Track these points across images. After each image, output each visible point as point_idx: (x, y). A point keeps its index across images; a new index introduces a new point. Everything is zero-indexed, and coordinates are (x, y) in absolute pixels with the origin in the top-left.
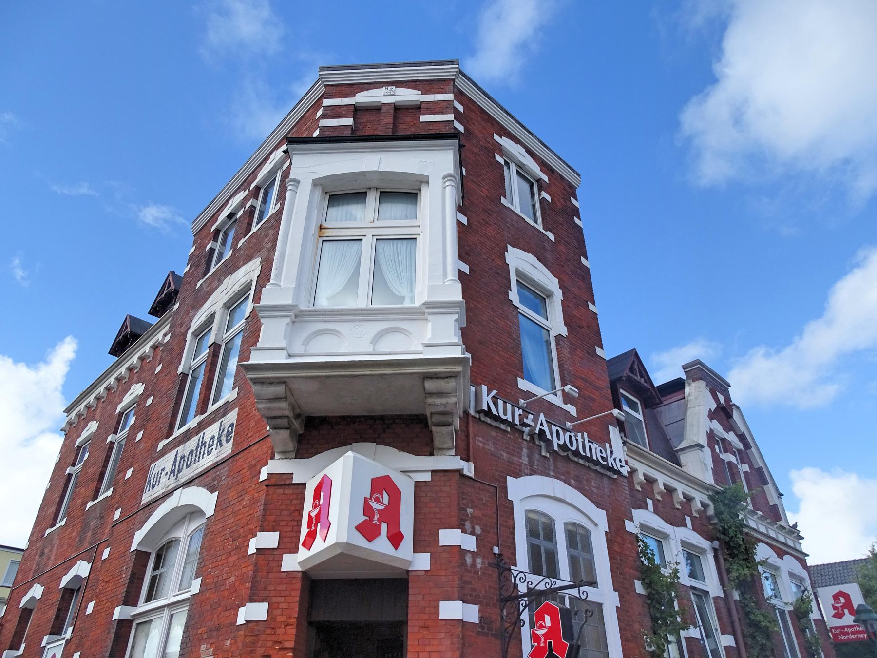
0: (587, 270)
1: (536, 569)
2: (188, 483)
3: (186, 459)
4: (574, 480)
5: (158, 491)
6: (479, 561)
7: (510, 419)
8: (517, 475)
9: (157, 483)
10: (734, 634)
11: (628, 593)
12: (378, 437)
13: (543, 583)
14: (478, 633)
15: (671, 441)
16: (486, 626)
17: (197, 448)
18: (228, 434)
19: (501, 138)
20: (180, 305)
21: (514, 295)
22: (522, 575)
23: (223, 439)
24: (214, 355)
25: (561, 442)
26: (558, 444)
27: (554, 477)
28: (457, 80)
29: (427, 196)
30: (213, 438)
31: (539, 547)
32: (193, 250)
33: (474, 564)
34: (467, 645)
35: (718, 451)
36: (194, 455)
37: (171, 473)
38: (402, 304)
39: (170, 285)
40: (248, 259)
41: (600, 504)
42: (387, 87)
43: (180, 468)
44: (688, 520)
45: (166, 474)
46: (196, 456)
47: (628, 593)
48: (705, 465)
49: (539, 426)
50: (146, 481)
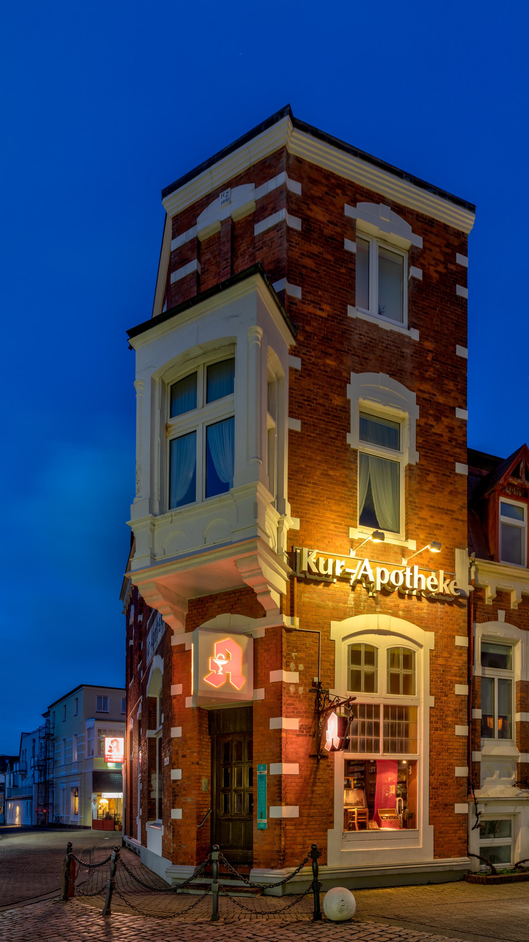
12: (232, 608)
14: (298, 735)
16: (305, 731)
25: (384, 582)
27: (380, 612)
28: (291, 145)
29: (401, 323)
31: (359, 672)
33: (296, 692)
34: (289, 743)
38: (501, 514)
41: (429, 627)
42: (223, 193)
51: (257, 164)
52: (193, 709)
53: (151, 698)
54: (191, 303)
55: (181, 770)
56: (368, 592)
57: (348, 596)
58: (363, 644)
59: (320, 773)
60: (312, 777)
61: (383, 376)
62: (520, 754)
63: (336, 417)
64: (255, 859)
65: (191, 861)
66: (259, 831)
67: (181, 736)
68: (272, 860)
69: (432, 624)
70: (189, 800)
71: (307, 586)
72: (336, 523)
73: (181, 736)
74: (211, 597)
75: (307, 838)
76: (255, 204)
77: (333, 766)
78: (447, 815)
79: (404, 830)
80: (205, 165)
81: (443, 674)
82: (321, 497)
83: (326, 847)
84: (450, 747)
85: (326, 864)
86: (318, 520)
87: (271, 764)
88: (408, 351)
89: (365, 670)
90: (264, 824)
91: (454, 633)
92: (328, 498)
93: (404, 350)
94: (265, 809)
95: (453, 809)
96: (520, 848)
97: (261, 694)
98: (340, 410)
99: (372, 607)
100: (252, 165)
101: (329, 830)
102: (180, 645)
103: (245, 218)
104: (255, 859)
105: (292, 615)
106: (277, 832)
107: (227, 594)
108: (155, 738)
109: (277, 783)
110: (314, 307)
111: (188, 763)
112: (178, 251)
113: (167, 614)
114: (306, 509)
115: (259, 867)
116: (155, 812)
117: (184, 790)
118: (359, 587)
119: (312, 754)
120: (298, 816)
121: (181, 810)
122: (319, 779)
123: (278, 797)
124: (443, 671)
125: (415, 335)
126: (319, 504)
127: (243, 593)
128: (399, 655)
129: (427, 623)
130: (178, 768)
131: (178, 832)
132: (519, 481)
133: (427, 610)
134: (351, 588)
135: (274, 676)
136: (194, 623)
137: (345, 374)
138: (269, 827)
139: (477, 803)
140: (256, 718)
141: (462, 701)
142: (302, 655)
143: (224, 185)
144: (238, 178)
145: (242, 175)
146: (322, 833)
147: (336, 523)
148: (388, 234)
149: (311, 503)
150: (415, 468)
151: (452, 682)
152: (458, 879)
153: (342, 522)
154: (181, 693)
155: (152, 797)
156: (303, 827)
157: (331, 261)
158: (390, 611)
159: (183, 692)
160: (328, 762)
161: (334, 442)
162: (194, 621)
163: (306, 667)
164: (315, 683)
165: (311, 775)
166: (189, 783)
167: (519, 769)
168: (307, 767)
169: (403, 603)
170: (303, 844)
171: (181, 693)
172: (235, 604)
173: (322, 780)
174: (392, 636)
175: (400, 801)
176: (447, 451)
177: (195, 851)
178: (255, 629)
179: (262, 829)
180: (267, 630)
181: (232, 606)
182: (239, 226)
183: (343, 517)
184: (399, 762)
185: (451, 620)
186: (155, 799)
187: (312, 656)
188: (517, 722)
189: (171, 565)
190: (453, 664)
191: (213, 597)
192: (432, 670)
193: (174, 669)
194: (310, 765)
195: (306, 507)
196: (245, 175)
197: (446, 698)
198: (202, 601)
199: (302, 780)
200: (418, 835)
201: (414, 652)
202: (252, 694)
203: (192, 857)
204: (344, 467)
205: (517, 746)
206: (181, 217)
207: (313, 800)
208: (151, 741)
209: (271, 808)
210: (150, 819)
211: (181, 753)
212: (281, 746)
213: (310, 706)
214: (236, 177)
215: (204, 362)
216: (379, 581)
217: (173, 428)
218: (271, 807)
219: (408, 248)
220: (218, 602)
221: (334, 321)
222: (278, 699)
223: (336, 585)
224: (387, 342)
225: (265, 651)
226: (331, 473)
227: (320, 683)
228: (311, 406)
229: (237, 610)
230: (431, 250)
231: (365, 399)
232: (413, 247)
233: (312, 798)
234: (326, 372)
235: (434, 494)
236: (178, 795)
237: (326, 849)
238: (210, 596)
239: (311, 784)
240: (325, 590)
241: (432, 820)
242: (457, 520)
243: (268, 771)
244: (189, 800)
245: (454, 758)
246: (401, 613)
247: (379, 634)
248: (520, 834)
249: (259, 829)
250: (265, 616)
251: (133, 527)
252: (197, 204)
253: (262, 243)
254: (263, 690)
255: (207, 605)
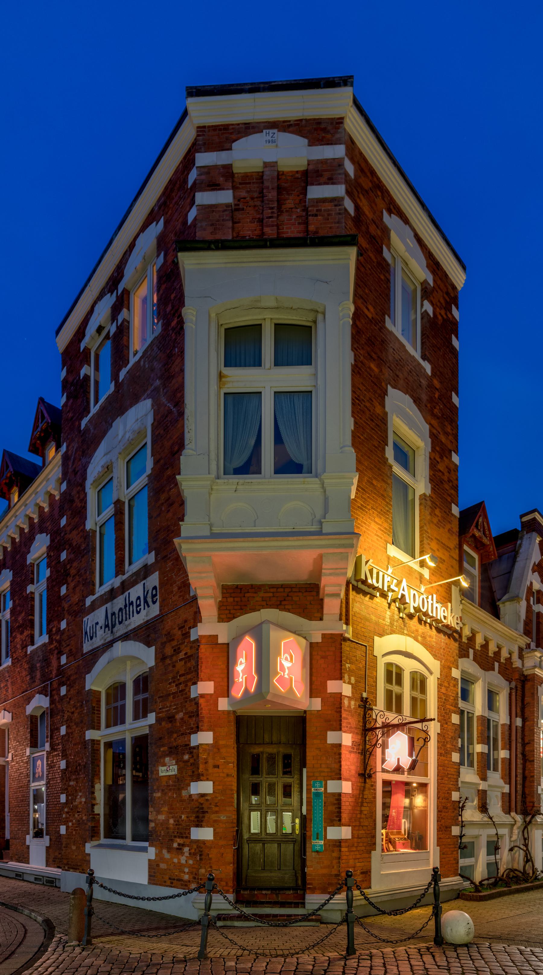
0: (454, 409)
1: (389, 708)
2: (125, 637)
3: (117, 616)
4: (421, 637)
5: (98, 642)
6: (353, 703)
7: (381, 587)
8: (381, 635)
9: (94, 635)
10: (510, 750)
11: (447, 723)
12: (280, 604)
13: (397, 719)
15: (495, 593)
17: (126, 606)
18: (154, 596)
19: (390, 216)
20: (67, 447)
21: (389, 453)
22: (382, 713)
23: (149, 600)
24: (119, 513)
25: (416, 605)
26: (414, 607)
30: (139, 598)
32: (64, 373)
35: (532, 603)
36: (124, 612)
37: (105, 628)
39: (43, 418)
40: (136, 399)
41: (436, 656)
42: (268, 131)
43: (114, 623)
44: (496, 665)
45: (101, 628)
46: (126, 614)
47: (447, 723)
48: (519, 616)
49: (401, 592)
50: (82, 633)
51: (310, 120)
52: (228, 712)
53: (95, 691)
54: (268, 243)
55: (211, 783)
56: (399, 612)
57: (386, 613)
58: (395, 664)
59: (366, 792)
60: (361, 796)
61: (408, 398)
62: (481, 782)
63: (378, 425)
64: (310, 884)
65: (226, 888)
66: (313, 854)
67: (212, 742)
68: (330, 884)
69: (438, 653)
70: (223, 818)
71: (358, 596)
72: (378, 536)
73: (212, 742)
74: (252, 586)
75: (357, 861)
76: (306, 163)
77: (375, 786)
78: (447, 837)
79: (417, 851)
80: (247, 87)
81: (444, 703)
82: (368, 505)
83: (371, 869)
84: (449, 772)
85: (370, 887)
86: (366, 528)
87: (328, 782)
88: (424, 382)
89: (396, 690)
90: (321, 845)
91: (451, 665)
92: (372, 508)
93: (421, 380)
94: (322, 830)
95: (451, 831)
96: (481, 866)
97: (317, 704)
98: (381, 420)
99: (402, 628)
100: (304, 118)
101: (372, 852)
102: (210, 636)
103: (292, 172)
104: (310, 884)
105: (347, 623)
106: (335, 854)
107: (272, 586)
108: (99, 741)
109: (336, 802)
110: (362, 303)
111: (221, 775)
112: (206, 170)
113: (205, 597)
114: (357, 514)
115: (314, 893)
116: (99, 830)
117: (216, 806)
118: (393, 606)
119: (361, 772)
120: (351, 838)
121: (211, 830)
122: (366, 799)
123: (337, 817)
124: (445, 699)
125: (428, 367)
126: (367, 512)
127: (294, 590)
128: (417, 679)
129: (435, 652)
130: (208, 780)
131: (208, 855)
132: (479, 533)
133: (436, 639)
134: (387, 605)
135: (332, 686)
136: (230, 613)
137: (383, 384)
138: (326, 850)
139: (464, 826)
140: (311, 729)
141: (456, 730)
142: (353, 667)
143: (269, 122)
144: (286, 124)
145: (292, 123)
146: (367, 855)
147: (378, 536)
148: (410, 258)
149: (361, 509)
150: (428, 499)
151: (450, 711)
152: (454, 897)
153: (382, 536)
154: (212, 692)
155: (96, 812)
156: (354, 849)
157: (374, 262)
158: (413, 635)
159: (215, 691)
160: (372, 782)
161: (377, 452)
162: (229, 610)
163: (356, 681)
164: (363, 698)
165: (359, 794)
166: (223, 798)
167: (480, 796)
168: (357, 786)
169: (422, 629)
170: (354, 867)
171: (212, 692)
172: (285, 600)
173: (367, 801)
174: (413, 660)
175: (405, 822)
176: (447, 490)
177: (232, 876)
178: (311, 632)
179: (317, 852)
180: (324, 636)
181: (281, 601)
182: (284, 177)
183: (383, 531)
184: (407, 784)
185: (449, 652)
186: (99, 815)
187: (360, 670)
188: (477, 753)
189: (243, 541)
190: (450, 694)
191: (255, 588)
192: (439, 698)
193: (202, 663)
194: (359, 784)
195: (358, 512)
196: (296, 125)
197: (446, 726)
198: (241, 589)
199: (353, 800)
200: (429, 856)
201: (427, 678)
202: (308, 703)
203: (227, 883)
204: (383, 480)
205: (478, 774)
206: (209, 131)
207: (362, 820)
208: (94, 744)
209: (329, 828)
210: (93, 839)
211: (211, 762)
212: (340, 762)
213: (359, 721)
214: (284, 122)
215: (272, 317)
216: (412, 604)
217: (228, 379)
218: (328, 828)
219: (422, 281)
220: (261, 594)
221: (376, 326)
222: (337, 712)
223: (378, 600)
224: (411, 367)
225: (323, 657)
226: (375, 482)
227: (367, 699)
228: (360, 406)
229: (287, 607)
230: (437, 291)
231: (397, 417)
232: (425, 281)
233: (360, 818)
234: (371, 376)
235: (439, 528)
236: (207, 812)
237: (370, 872)
238: (252, 585)
239: (360, 804)
240: (370, 603)
241: (440, 842)
242: (453, 557)
243: (326, 789)
244: (223, 818)
245: (452, 783)
246: (420, 638)
247: (405, 656)
248: (481, 854)
249: (314, 852)
250: (321, 619)
251: (183, 483)
252: (231, 127)
253: (317, 210)
254: (319, 700)
255: (247, 595)
